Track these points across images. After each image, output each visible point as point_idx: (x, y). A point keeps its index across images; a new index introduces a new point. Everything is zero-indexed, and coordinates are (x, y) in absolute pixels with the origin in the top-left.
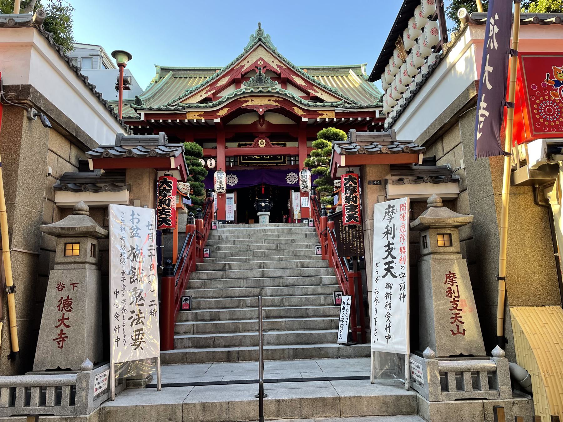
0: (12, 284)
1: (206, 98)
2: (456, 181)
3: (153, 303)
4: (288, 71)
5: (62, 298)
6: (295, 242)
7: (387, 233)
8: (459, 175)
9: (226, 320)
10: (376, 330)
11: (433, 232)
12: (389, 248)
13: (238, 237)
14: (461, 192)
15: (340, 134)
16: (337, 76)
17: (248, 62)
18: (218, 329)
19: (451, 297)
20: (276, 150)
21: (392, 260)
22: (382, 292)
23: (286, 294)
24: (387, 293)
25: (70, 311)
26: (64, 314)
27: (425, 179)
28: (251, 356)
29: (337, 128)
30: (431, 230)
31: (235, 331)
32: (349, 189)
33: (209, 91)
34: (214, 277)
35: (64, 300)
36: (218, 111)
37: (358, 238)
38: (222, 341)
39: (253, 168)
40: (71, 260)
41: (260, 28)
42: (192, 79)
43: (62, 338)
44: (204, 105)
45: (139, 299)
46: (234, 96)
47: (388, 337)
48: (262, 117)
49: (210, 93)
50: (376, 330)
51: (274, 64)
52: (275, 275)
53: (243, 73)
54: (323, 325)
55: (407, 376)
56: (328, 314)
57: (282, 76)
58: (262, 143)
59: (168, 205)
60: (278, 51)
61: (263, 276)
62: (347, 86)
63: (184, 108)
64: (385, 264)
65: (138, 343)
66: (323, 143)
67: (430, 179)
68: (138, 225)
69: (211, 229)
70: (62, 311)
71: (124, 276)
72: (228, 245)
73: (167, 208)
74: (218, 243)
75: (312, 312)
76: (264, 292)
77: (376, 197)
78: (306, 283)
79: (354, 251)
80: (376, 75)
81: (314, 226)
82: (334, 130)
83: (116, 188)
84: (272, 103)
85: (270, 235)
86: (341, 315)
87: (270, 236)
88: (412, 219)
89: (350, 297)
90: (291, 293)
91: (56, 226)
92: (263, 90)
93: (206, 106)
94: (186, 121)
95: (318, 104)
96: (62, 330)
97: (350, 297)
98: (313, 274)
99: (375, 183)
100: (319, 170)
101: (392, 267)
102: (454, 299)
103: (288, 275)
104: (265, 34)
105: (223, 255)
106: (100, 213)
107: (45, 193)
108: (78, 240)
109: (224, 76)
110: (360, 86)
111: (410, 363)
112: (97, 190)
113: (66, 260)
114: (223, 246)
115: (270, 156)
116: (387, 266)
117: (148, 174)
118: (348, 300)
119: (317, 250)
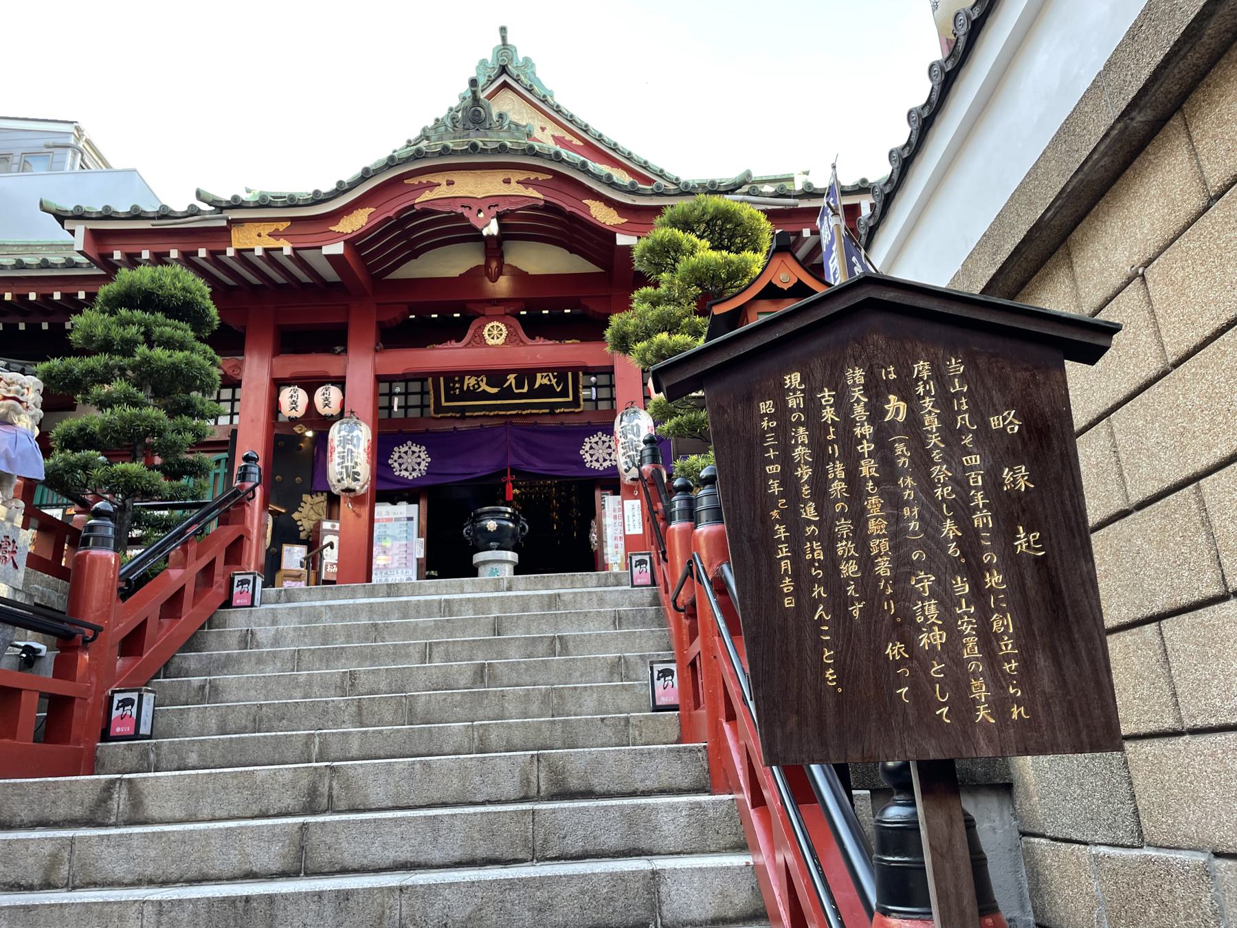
6: (565, 650)
15: (745, 214)
37: (955, 568)
39: (477, 423)
48: (494, 248)
58: (495, 333)
60: (559, 99)
69: (228, 604)
72: (269, 672)
81: (654, 583)
84: (516, 189)
85: (465, 625)
94: (230, 252)
103: (458, 854)
119: (659, 684)
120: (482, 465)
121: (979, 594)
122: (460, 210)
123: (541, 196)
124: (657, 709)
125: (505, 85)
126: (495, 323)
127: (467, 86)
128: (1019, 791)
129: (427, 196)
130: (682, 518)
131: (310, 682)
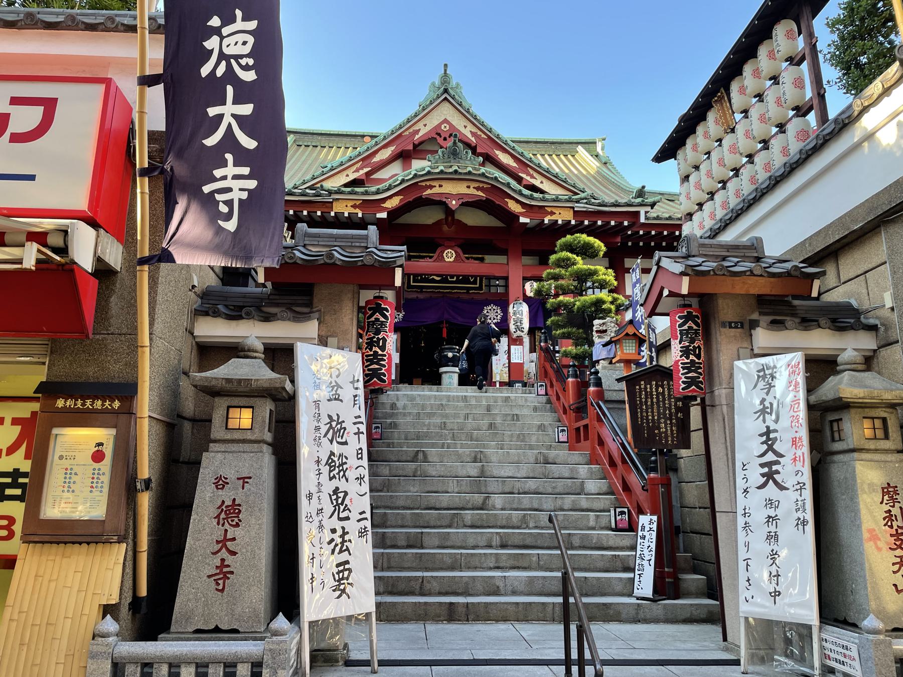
0: (146, 476)
1: (355, 179)
2: (873, 328)
3: (363, 516)
5: (223, 502)
6: (518, 420)
7: (763, 412)
8: (877, 318)
9: (433, 548)
10: (748, 580)
11: (856, 413)
12: (768, 439)
13: (423, 407)
14: (879, 348)
15: (596, 245)
16: (558, 155)
17: (425, 125)
18: (424, 563)
19: (891, 527)
20: (472, 267)
21: (775, 458)
22: (759, 516)
23: (527, 507)
24: (769, 517)
25: (237, 525)
26: (226, 531)
27: (823, 322)
28: (488, 612)
29: (588, 236)
30: (853, 411)
31: (452, 568)
32: (687, 334)
33: (361, 168)
34: (400, 472)
35: (227, 507)
36: (384, 200)
38: (435, 584)
39: (428, 295)
40: (237, 436)
41: (445, 73)
42: (325, 150)
43: (223, 573)
44: (349, 189)
45: (342, 508)
46: (413, 178)
47: (776, 594)
49: (362, 172)
50: (748, 580)
51: (467, 131)
52: (503, 474)
53: (416, 143)
54: (600, 564)
55: (817, 664)
56: (605, 545)
58: (449, 256)
59: (383, 348)
60: (473, 110)
61: (482, 474)
62: (576, 172)
63: (330, 192)
64: (762, 465)
65: (342, 587)
66: (568, 259)
67: (829, 323)
68: (339, 381)
70: (223, 525)
71: (320, 467)
72: (409, 419)
73: (380, 352)
74: (392, 415)
75: (578, 541)
76: (490, 503)
77: (735, 350)
78: (557, 491)
79: (661, 439)
80: (668, 152)
81: (546, 394)
82: (584, 237)
83: (300, 317)
84: (472, 191)
85: (476, 407)
86: (639, 547)
87: (476, 408)
88: (810, 390)
89: (655, 518)
90: (536, 506)
91: (215, 376)
92: (460, 171)
93: (366, 191)
94: (332, 214)
95: (536, 195)
96: (223, 560)
97: (655, 518)
98: (567, 475)
99: (733, 325)
100: (561, 302)
101: (777, 472)
102: (897, 530)
104: (453, 83)
105: (403, 437)
106: (281, 356)
107: (185, 322)
108: (251, 401)
109: (385, 146)
110: (598, 172)
111: (821, 640)
112: (267, 318)
113: (229, 436)
114: (400, 421)
115: (458, 276)
116: (766, 470)
117: (350, 295)
118: (651, 522)
119: (560, 434)
120: (430, 318)
121: (671, 423)
122: (444, 200)
124: (559, 442)
128: (679, 473)
130: (573, 377)
131: (429, 424)
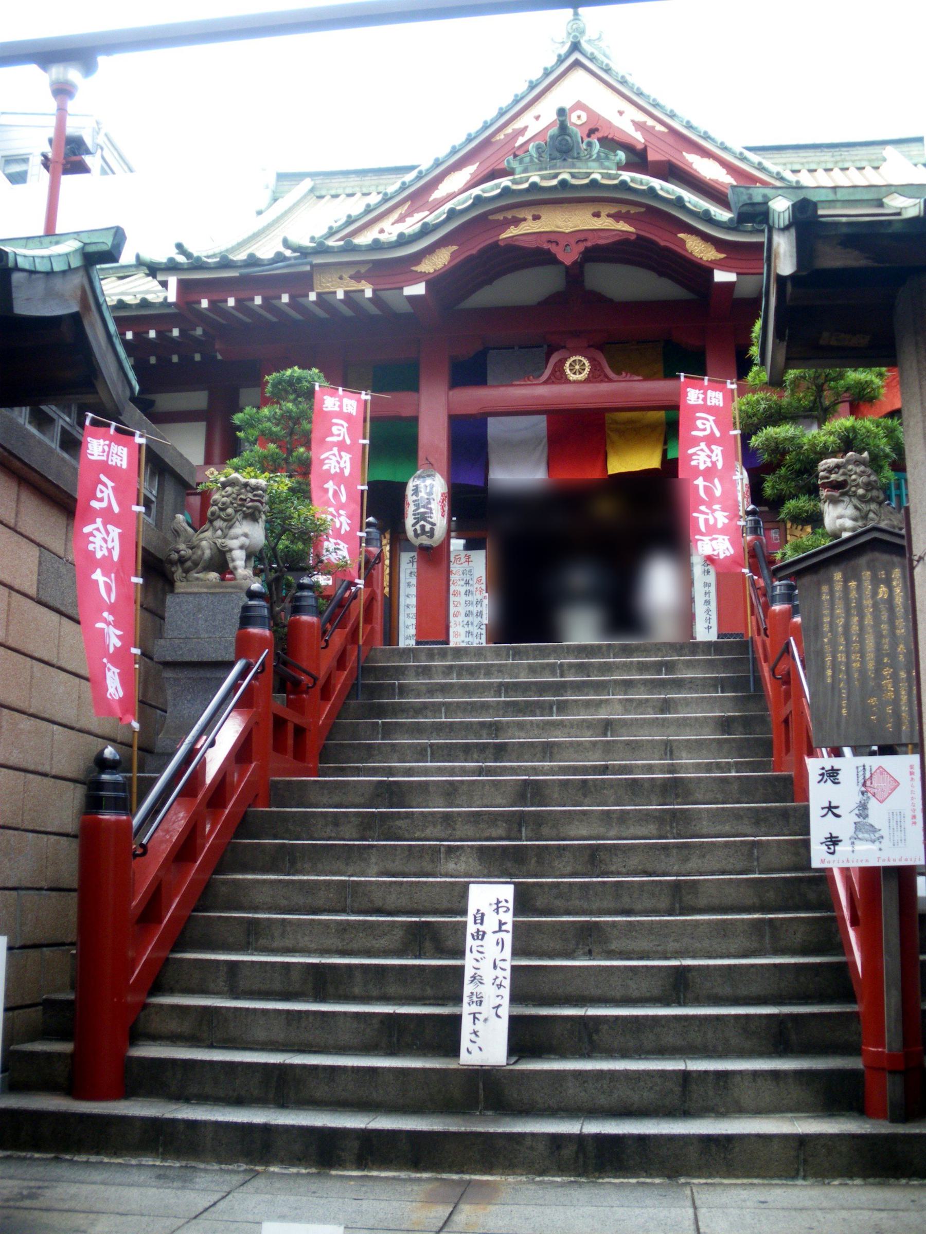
4: (671, 140)
17: (537, 118)
33: (409, 214)
36: (418, 257)
51: (626, 122)
57: (652, 156)
84: (605, 223)
94: (312, 297)
123: (632, 229)
125: (577, 64)
126: (578, 358)
127: (555, 117)
129: (512, 232)
